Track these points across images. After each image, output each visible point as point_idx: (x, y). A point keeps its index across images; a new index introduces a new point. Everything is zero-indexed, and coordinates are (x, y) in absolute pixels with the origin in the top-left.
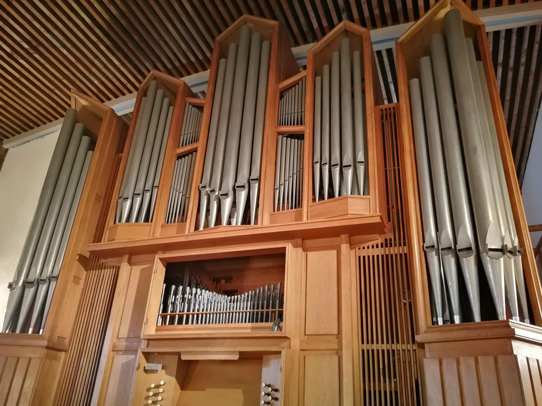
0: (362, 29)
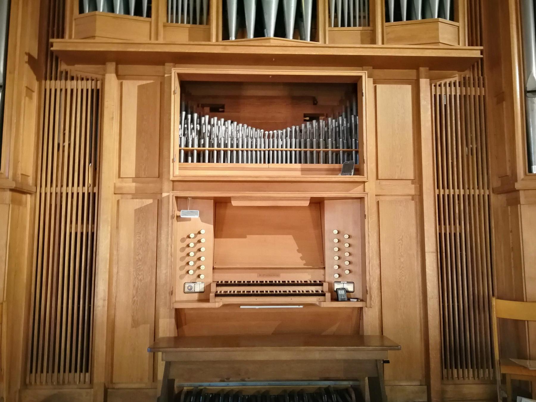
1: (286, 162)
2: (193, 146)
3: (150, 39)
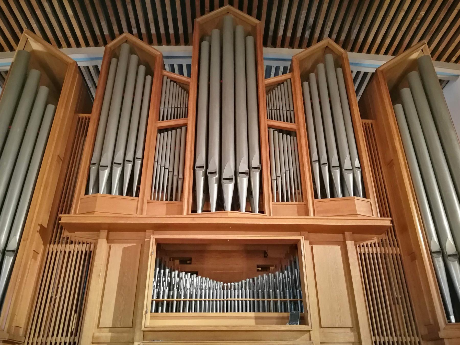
0: (342, 50)
1: (242, 311)
2: (163, 297)
3: (137, 213)
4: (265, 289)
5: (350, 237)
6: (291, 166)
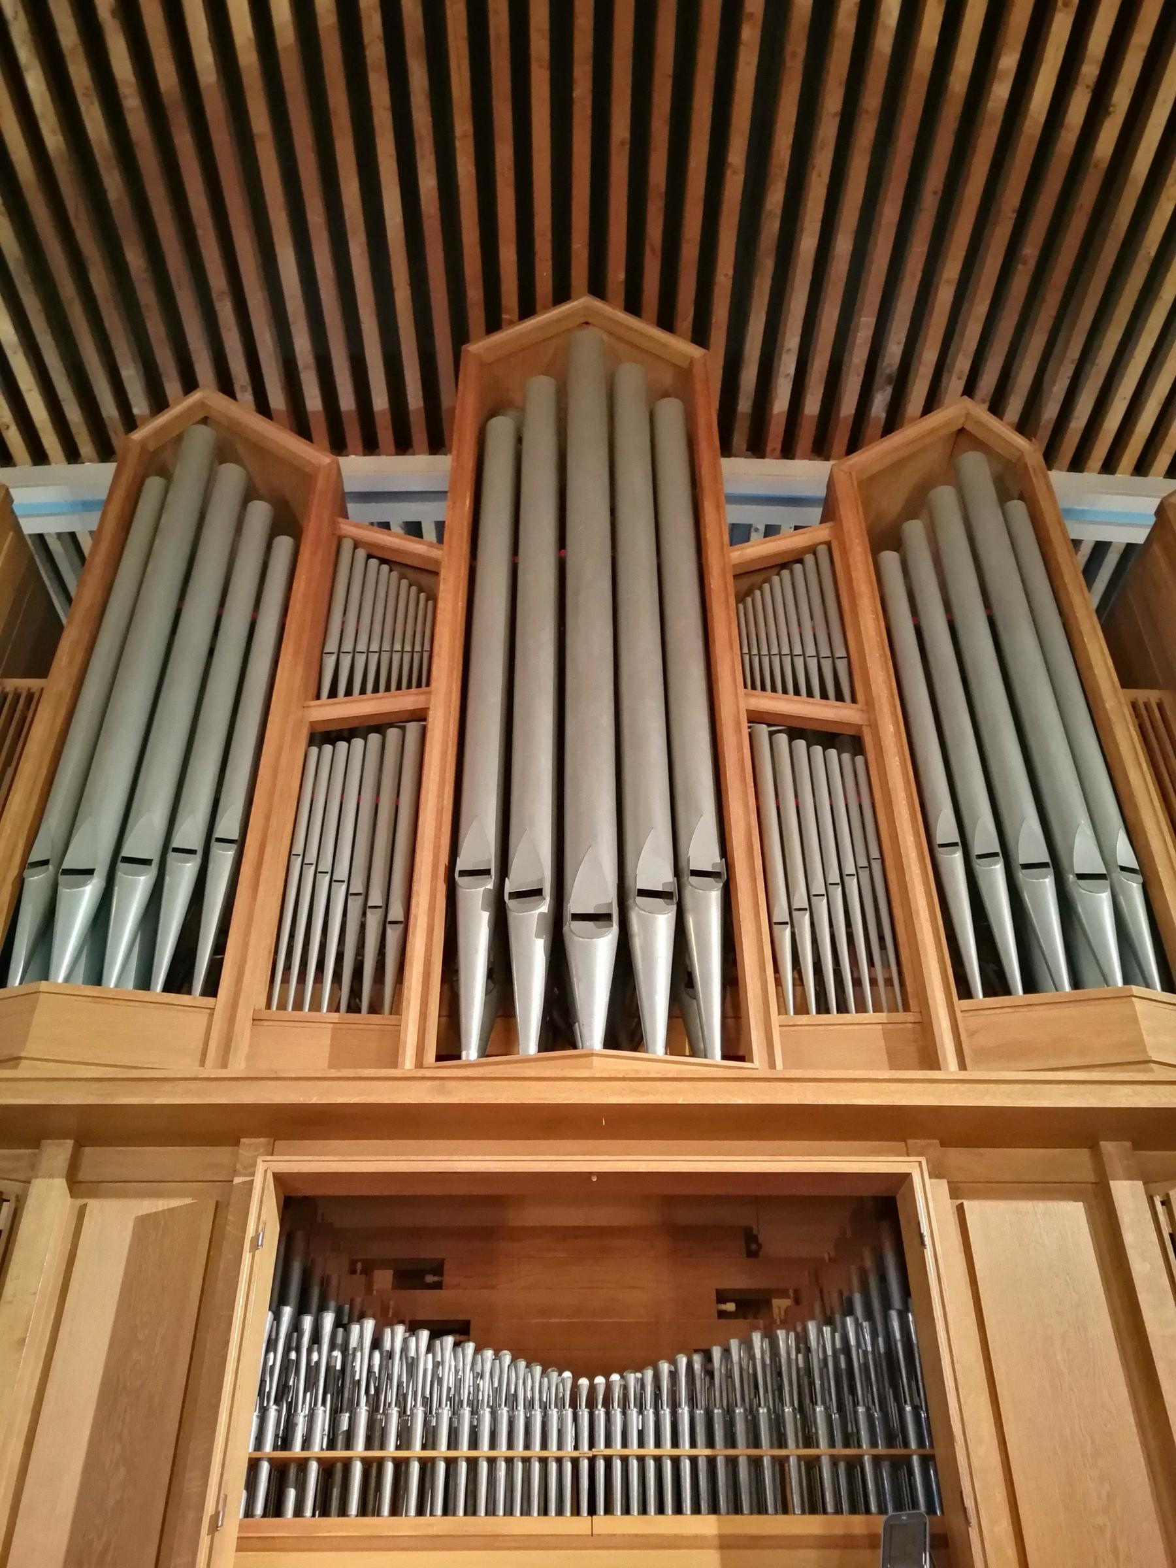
2: (307, 1443)
3: (202, 1062)
4: (762, 1404)
5: (1125, 1162)
6: (850, 868)
